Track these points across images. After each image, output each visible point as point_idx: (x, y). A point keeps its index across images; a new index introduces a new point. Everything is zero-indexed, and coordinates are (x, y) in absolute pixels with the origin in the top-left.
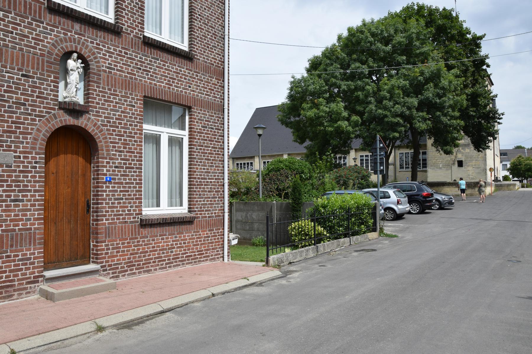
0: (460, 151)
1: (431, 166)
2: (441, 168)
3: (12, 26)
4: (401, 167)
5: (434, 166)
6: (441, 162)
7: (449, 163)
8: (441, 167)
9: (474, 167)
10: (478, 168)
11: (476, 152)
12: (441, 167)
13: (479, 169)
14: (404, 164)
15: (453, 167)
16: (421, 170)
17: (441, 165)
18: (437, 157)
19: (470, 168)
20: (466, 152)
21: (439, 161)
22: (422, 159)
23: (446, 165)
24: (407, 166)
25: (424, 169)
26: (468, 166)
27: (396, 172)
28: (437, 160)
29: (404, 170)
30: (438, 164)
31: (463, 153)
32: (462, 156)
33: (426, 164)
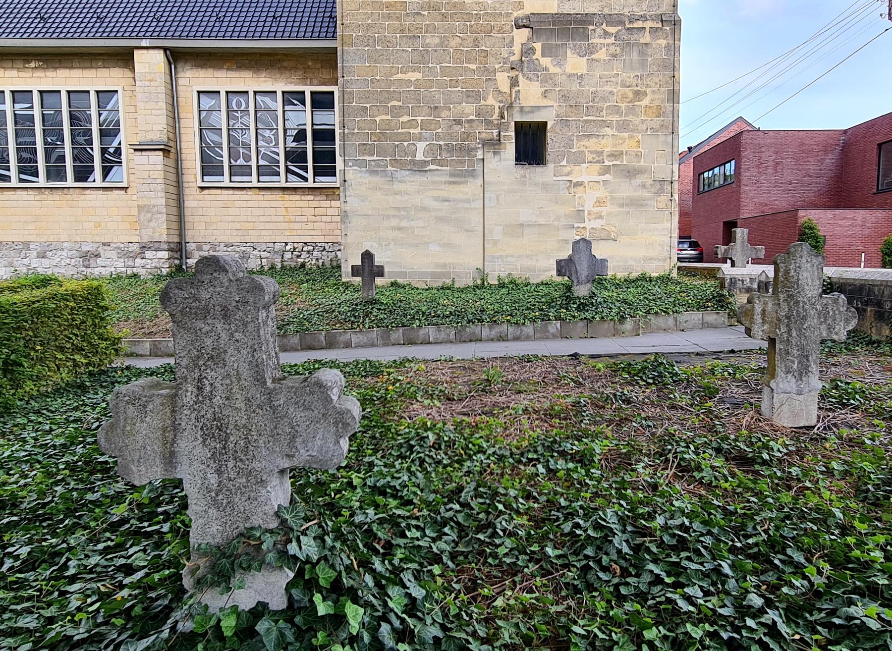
0: (535, 67)
1: (365, 149)
2: (419, 168)
3: (698, 648)
4: (210, 167)
5: (382, 152)
6: (424, 125)
7: (468, 136)
8: (420, 157)
9: (607, 170)
10: (630, 173)
11: (539, 169)
12: (420, 157)
13: (639, 180)
14: (225, 153)
15: (492, 162)
16: (310, 184)
17: (421, 146)
18: (396, 95)
19: (585, 173)
20: (569, 69)
21: (412, 124)
22: (315, 132)
23: (451, 149)
24: (241, 162)
25: (325, 181)
26: (578, 159)
27: (187, 191)
28: (395, 112)
29: (225, 181)
30: (408, 137)
31: (546, 78)
32: (545, 95)
33: (331, 156)
